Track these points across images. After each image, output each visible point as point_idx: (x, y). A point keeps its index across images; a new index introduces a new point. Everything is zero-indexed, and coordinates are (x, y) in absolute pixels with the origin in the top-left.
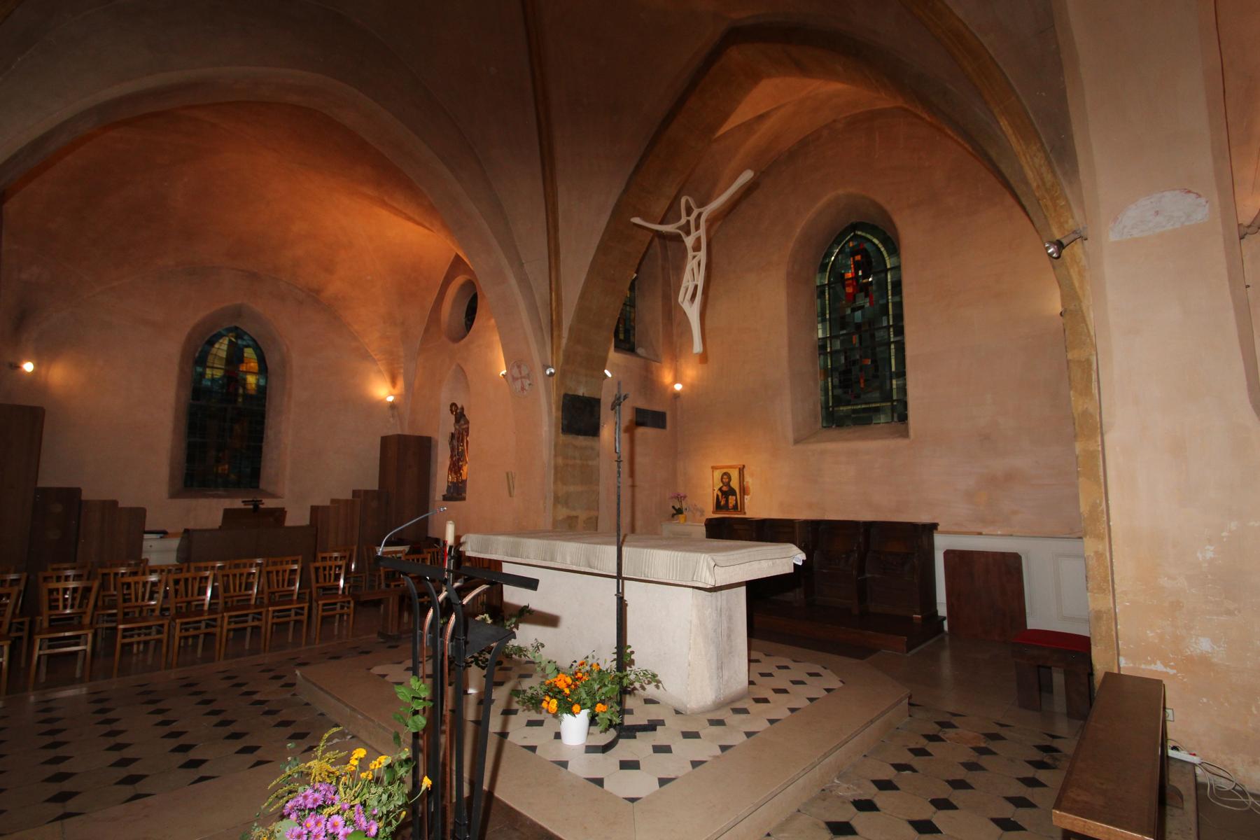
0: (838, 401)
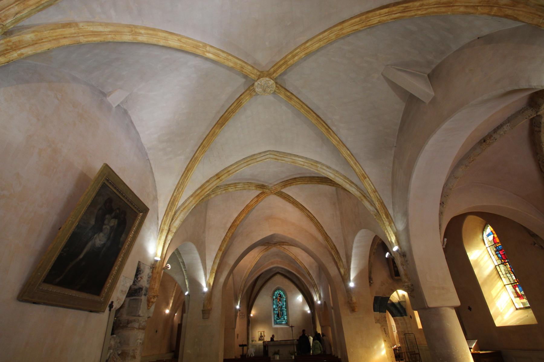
0: (277, 319)
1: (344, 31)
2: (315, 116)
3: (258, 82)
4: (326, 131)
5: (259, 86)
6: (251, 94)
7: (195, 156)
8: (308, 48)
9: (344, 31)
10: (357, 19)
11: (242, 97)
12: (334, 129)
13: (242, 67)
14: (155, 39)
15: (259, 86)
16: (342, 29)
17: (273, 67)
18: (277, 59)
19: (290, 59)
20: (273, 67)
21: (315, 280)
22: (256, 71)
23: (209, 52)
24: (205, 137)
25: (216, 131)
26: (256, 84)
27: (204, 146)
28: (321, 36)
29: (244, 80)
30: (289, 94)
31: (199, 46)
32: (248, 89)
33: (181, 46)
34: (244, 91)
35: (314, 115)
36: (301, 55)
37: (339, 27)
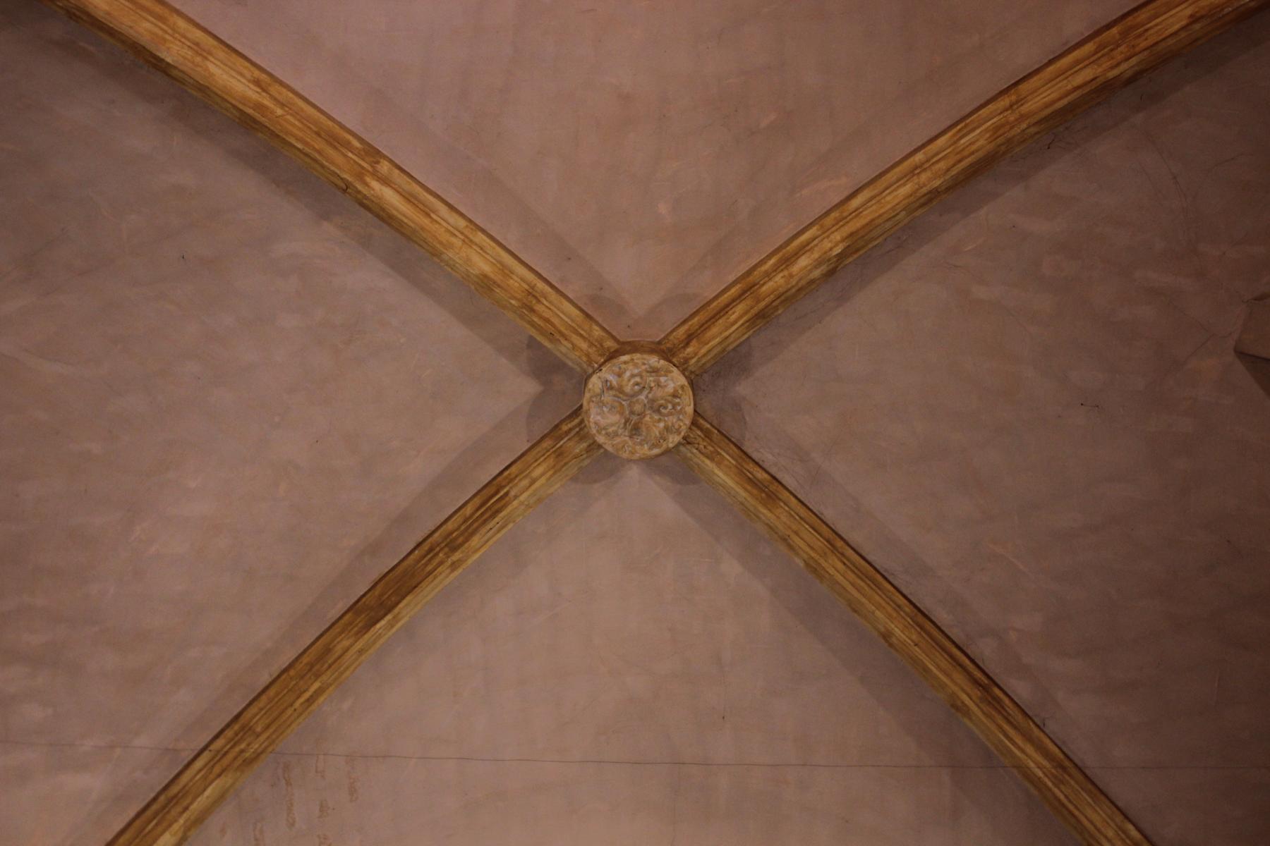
1: (1025, 108)
2: (908, 608)
3: (607, 374)
4: (977, 693)
5: (608, 397)
6: (560, 454)
7: (175, 789)
8: (857, 212)
9: (1025, 108)
10: (1089, 47)
11: (513, 469)
12: (1021, 689)
13: (531, 293)
14: (147, 25)
15: (608, 397)
16: (1020, 101)
17: (685, 322)
18: (707, 286)
19: (769, 275)
20: (685, 322)
21: (771, 284)
22: (597, 332)
23: (385, 181)
24: (265, 679)
25: (338, 650)
26: (595, 383)
27: (247, 729)
28: (919, 157)
29: (531, 387)
30: (761, 475)
31: (347, 145)
32: (554, 432)
33: (259, 107)
34: (526, 446)
35: (902, 601)
36: (827, 245)
37: (1004, 102)
